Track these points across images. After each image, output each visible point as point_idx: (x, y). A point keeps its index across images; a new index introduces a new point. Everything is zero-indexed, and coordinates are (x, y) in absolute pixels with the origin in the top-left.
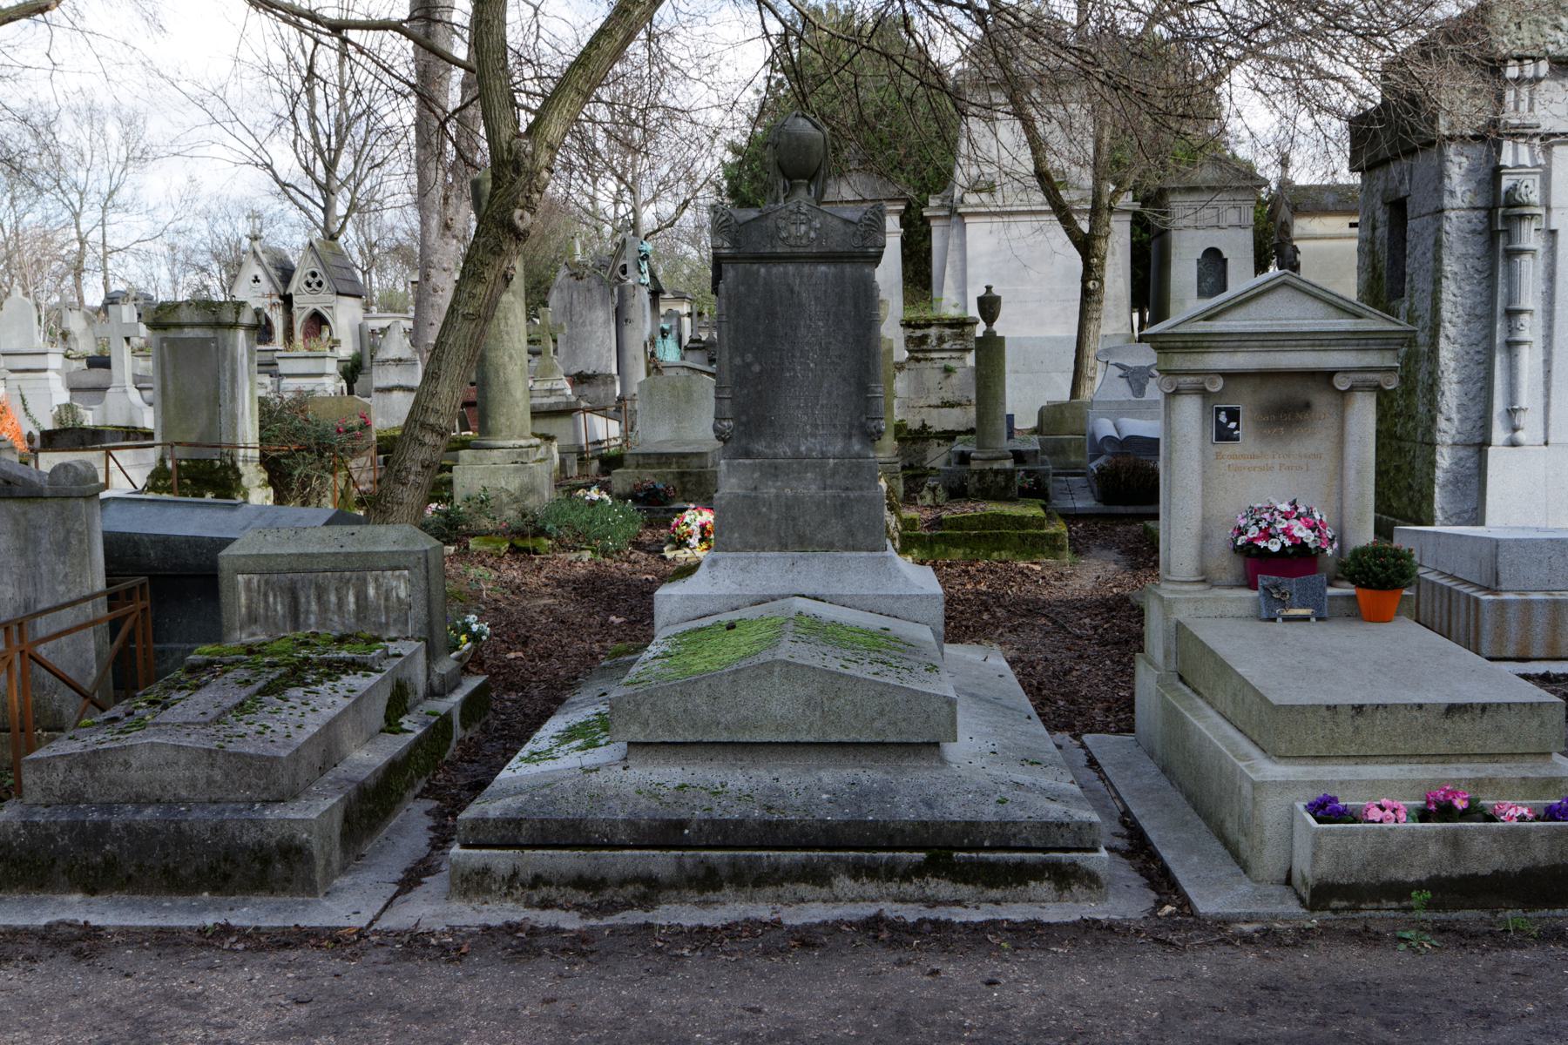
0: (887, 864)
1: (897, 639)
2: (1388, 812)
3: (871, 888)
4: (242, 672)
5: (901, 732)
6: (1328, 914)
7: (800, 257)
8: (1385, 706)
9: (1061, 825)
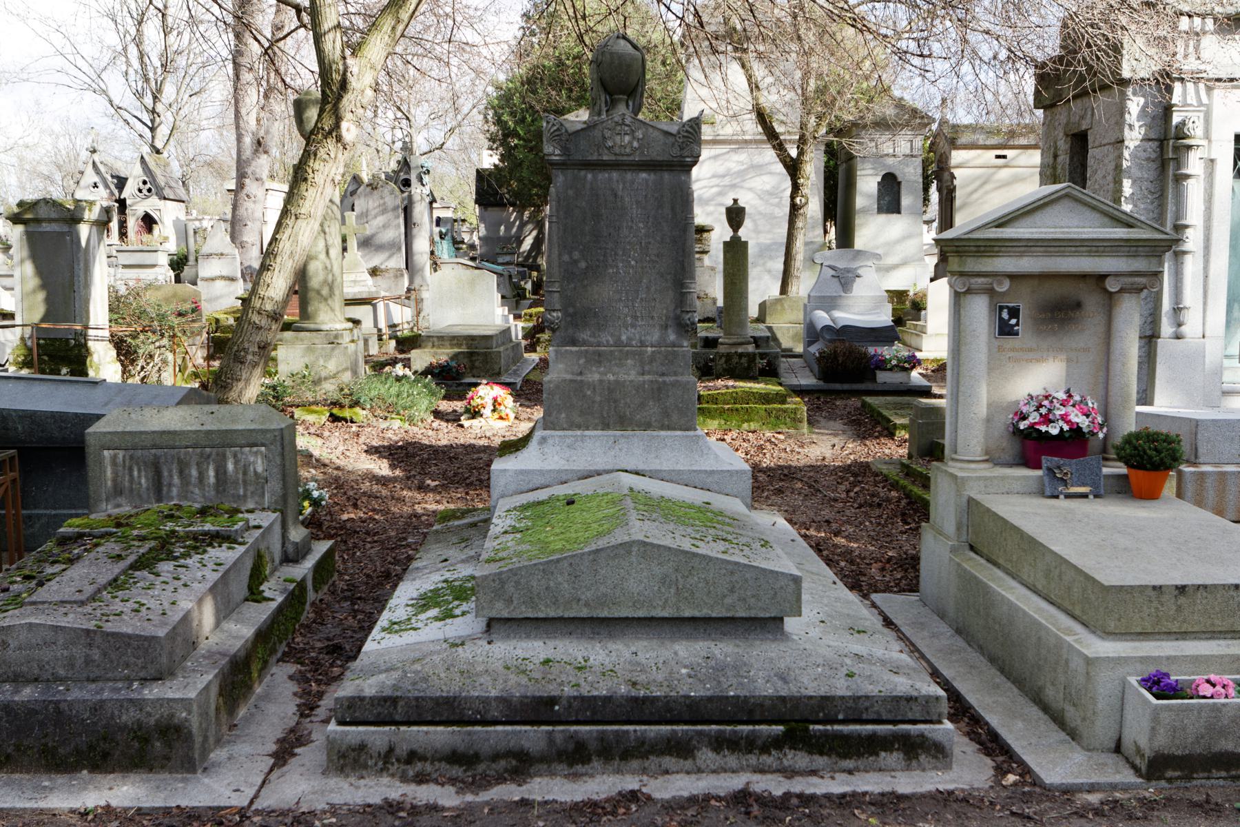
0: (747, 737)
1: (721, 513)
2: (1219, 688)
3: (732, 760)
4: (113, 545)
5: (750, 608)
6: (1163, 783)
7: (623, 165)
8: (1205, 587)
9: (910, 699)
